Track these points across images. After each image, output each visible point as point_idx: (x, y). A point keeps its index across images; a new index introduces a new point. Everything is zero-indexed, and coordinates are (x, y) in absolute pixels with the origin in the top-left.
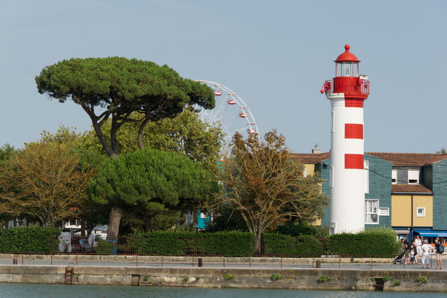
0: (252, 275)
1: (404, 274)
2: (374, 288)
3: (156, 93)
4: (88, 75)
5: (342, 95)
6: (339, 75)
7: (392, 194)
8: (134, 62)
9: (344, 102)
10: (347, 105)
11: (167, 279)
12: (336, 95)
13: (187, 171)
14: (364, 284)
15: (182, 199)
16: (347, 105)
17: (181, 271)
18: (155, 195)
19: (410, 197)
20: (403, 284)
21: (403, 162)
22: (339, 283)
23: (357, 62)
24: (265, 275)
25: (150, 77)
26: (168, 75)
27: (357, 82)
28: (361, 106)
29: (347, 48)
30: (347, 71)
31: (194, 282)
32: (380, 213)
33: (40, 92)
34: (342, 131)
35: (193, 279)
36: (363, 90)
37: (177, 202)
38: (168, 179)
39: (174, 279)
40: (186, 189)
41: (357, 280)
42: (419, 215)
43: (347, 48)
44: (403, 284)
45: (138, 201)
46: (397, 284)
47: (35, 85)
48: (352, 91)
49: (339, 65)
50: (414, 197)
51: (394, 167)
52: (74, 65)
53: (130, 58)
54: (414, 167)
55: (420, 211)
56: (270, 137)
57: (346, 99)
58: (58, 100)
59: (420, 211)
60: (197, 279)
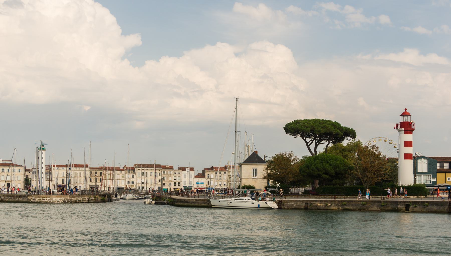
0: (354, 203)
1: (419, 202)
2: (45, 187)
3: (328, 132)
4: (302, 126)
5: (403, 129)
6: (402, 121)
7: (437, 172)
8: (323, 120)
9: (404, 132)
10: (405, 133)
11: (319, 204)
12: (401, 129)
13: (338, 162)
14: (401, 206)
15: (336, 173)
16: (405, 133)
17: (325, 201)
18: (324, 171)
19: (444, 174)
20: (418, 207)
21: (442, 160)
22: (390, 206)
23: (410, 115)
24: (359, 203)
25: (327, 125)
26: (336, 125)
27: (409, 124)
28: (411, 133)
29: (406, 110)
30: (406, 119)
31: (330, 206)
32: (432, 180)
33: (287, 133)
34: (403, 144)
35: (330, 204)
36: (413, 127)
37: (334, 174)
38: (330, 165)
39: (322, 205)
40: (337, 169)
41: (398, 205)
42: (448, 180)
43: (406, 110)
44: (418, 207)
45: (318, 174)
46: (416, 207)
47: (284, 131)
48: (407, 127)
49: (402, 117)
50: (446, 174)
51: (438, 162)
52: (297, 122)
53: (321, 119)
54: (446, 162)
55: (449, 179)
56: (373, 147)
57: (405, 131)
58: (294, 137)
59: (449, 179)
60: (331, 205)
